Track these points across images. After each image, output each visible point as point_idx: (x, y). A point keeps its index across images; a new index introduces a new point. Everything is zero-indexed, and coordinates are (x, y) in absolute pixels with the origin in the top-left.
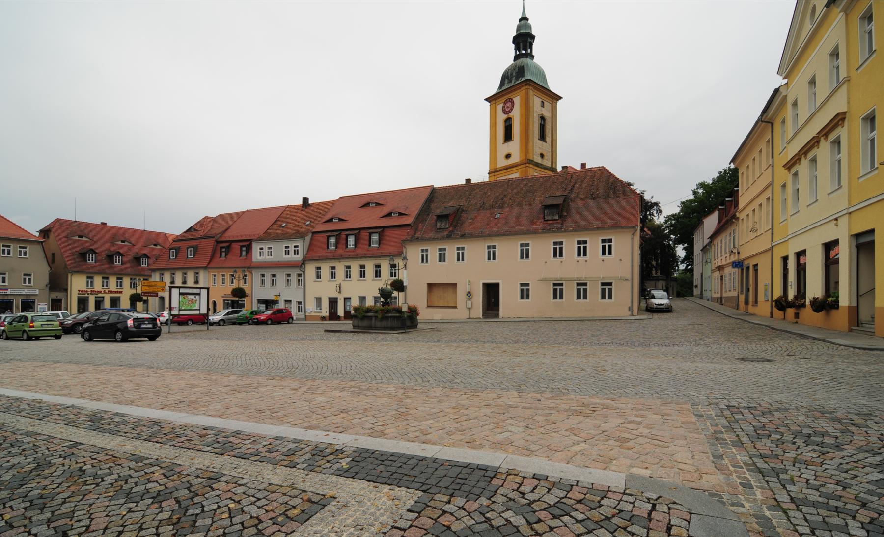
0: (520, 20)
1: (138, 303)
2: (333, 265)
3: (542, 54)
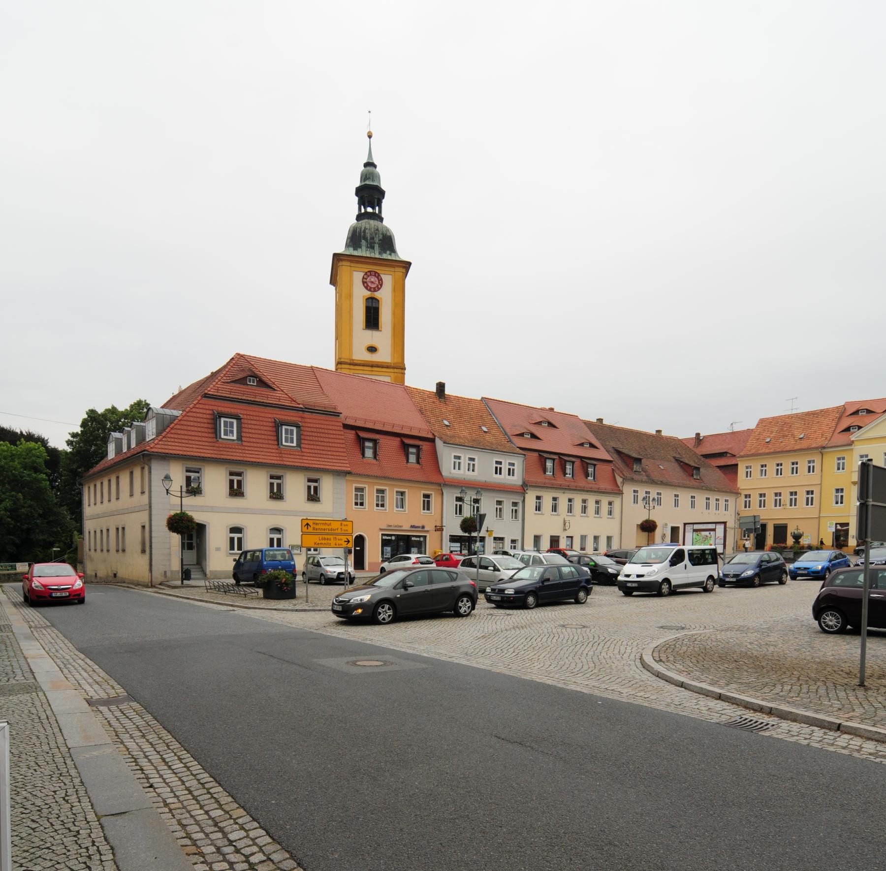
0: (366, 165)
1: (458, 545)
3: (393, 215)
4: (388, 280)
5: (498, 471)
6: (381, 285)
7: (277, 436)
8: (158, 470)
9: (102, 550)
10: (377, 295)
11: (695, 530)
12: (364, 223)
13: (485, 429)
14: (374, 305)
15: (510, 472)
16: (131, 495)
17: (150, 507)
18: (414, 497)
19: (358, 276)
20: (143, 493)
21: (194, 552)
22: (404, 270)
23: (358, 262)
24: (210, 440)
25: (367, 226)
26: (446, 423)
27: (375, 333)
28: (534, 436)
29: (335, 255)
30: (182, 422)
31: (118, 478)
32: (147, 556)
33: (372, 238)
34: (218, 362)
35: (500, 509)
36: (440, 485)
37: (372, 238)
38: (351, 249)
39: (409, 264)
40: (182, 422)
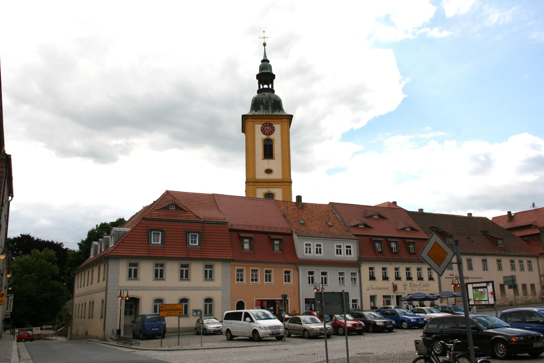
0: (262, 61)
2: (385, 266)
3: (280, 88)
4: (277, 127)
5: (339, 252)
6: (274, 131)
7: (186, 240)
8: (112, 265)
9: (81, 317)
10: (271, 137)
11: (474, 288)
12: (261, 95)
13: (330, 224)
14: (269, 144)
15: (349, 252)
16: (98, 282)
17: (107, 289)
18: (278, 273)
19: (258, 127)
20: (104, 280)
21: (133, 316)
22: (288, 120)
23: (258, 119)
24: (145, 245)
25: (264, 97)
26: (302, 222)
27: (271, 161)
28: (366, 226)
29: (243, 116)
30: (129, 236)
31: (93, 270)
32: (103, 320)
33: (267, 103)
34: (156, 196)
35: (343, 278)
36: (296, 264)
37: (267, 103)
38: (254, 112)
39: (292, 116)
40: (129, 236)
